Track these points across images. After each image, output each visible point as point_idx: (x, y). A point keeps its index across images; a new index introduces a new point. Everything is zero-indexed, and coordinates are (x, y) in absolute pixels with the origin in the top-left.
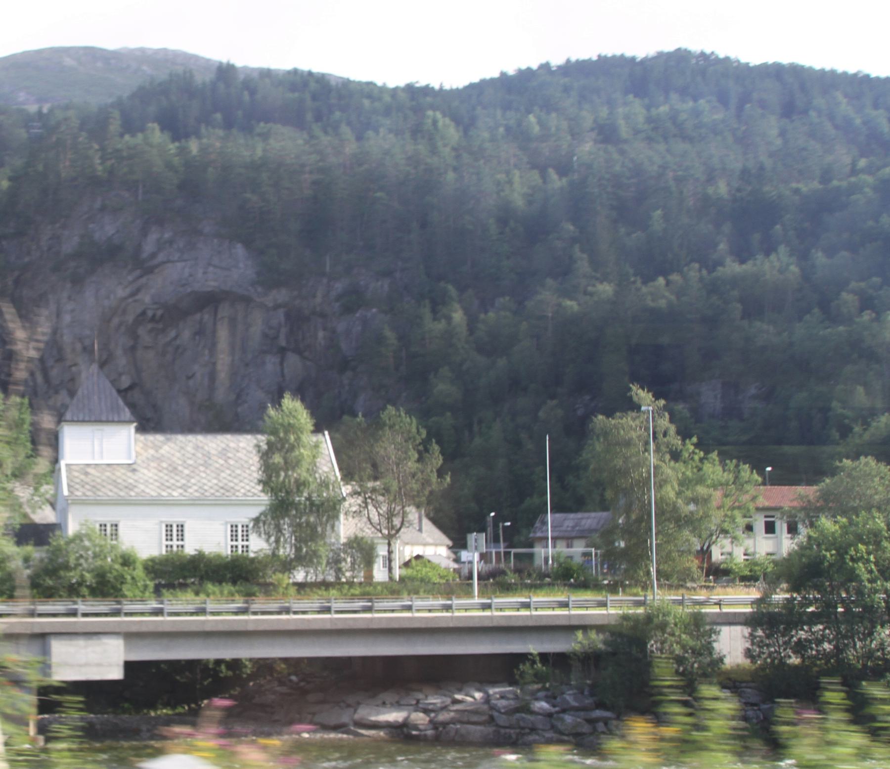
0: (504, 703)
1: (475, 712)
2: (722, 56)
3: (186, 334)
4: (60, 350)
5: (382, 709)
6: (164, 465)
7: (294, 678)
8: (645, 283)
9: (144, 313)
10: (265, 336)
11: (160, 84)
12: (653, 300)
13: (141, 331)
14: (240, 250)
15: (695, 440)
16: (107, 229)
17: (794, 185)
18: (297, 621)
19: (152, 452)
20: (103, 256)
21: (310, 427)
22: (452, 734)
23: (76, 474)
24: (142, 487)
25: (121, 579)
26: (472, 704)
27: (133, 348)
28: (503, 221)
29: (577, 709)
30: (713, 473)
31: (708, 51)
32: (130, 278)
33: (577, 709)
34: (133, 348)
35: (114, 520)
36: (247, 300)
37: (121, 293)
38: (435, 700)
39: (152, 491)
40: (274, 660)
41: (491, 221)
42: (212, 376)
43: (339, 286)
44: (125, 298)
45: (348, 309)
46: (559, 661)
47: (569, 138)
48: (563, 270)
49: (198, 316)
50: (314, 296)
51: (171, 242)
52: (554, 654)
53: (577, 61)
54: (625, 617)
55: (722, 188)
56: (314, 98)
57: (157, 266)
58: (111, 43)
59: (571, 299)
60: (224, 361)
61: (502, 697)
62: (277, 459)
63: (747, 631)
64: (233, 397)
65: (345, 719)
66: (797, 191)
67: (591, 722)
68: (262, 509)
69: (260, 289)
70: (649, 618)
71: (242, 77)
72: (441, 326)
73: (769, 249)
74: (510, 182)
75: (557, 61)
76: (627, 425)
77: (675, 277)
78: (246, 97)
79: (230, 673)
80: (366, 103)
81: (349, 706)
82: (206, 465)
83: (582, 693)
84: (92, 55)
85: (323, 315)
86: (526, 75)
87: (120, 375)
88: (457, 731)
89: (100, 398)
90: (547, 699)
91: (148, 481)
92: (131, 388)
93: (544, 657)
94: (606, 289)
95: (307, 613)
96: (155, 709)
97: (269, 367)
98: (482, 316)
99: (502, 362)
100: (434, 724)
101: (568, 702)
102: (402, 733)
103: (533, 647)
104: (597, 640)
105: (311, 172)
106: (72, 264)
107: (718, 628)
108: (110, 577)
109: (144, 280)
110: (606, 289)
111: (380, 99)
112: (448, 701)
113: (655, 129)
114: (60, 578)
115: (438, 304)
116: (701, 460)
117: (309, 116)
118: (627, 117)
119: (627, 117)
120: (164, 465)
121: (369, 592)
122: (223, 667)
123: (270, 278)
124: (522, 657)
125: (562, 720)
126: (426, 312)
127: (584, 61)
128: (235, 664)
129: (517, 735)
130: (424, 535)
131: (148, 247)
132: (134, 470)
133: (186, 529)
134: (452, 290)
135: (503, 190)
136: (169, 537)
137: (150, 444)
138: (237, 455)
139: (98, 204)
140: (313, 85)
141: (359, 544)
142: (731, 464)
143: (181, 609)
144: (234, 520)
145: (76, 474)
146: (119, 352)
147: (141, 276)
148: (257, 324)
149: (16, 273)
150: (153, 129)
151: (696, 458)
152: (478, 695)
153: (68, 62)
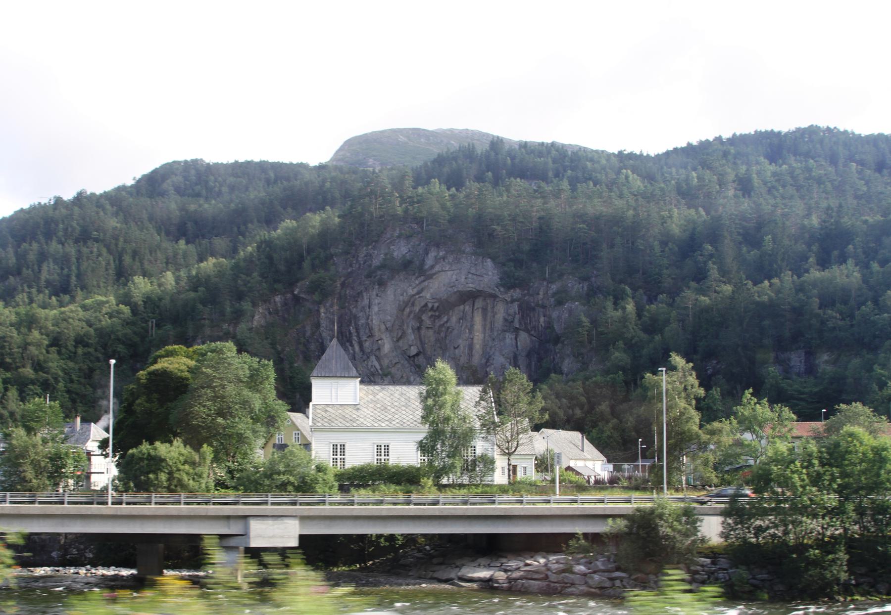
0: (556, 566)
1: (536, 572)
2: (842, 130)
3: (454, 319)
4: (371, 329)
5: (477, 569)
6: (379, 406)
7: (427, 547)
8: (755, 284)
9: (426, 305)
10: (506, 320)
11: (452, 153)
12: (759, 297)
13: (424, 317)
14: (489, 263)
15: (751, 390)
16: (401, 250)
17: (864, 218)
18: (440, 510)
19: (371, 397)
20: (409, 267)
21: (454, 380)
22: (519, 586)
23: (319, 411)
24: (362, 420)
25: (315, 481)
26: (537, 566)
27: (419, 329)
28: (664, 244)
29: (604, 571)
30: (763, 413)
31: (832, 127)
32: (417, 282)
33: (604, 571)
34: (419, 329)
35: (342, 442)
36: (494, 297)
37: (411, 292)
38: (513, 564)
39: (368, 423)
40: (59, 534)
41: (656, 243)
42: (471, 347)
43: (554, 287)
44: (414, 295)
45: (560, 303)
46: (594, 538)
47: (718, 187)
48: (700, 276)
49: (462, 307)
50: (538, 294)
51: (444, 258)
52: (592, 534)
53: (741, 135)
54: (638, 510)
55: (815, 221)
56: (554, 162)
57: (434, 274)
58: (431, 126)
59: (704, 295)
60: (478, 337)
61: (557, 562)
62: (430, 402)
63: (720, 519)
64: (484, 361)
65: (453, 575)
66: (866, 222)
67: (612, 579)
68: (424, 435)
69: (502, 289)
70: (652, 511)
71: (507, 147)
72: (619, 313)
73: (843, 260)
74: (671, 217)
75: (726, 135)
76: (664, 380)
77: (775, 281)
78: (509, 161)
79: (387, 544)
80: (589, 164)
81: (457, 567)
82: (406, 406)
83: (609, 560)
84: (417, 133)
85: (544, 307)
86: (705, 145)
87: (410, 346)
88: (523, 584)
89: (336, 362)
90: (585, 564)
91: (366, 416)
92: (417, 355)
93: (586, 535)
94: (728, 289)
95: (448, 504)
96: (338, 567)
97: (508, 341)
98: (647, 307)
99: (658, 338)
100: (509, 580)
101: (598, 566)
102: (488, 586)
103: (579, 528)
104: (622, 524)
105: (538, 211)
106: (379, 273)
107: (701, 517)
108: (308, 479)
109: (426, 283)
110: (728, 289)
111: (598, 162)
112: (521, 564)
113: (778, 181)
114: (273, 479)
115: (618, 299)
116: (755, 404)
117: (550, 174)
118: (759, 173)
119: (759, 173)
120: (379, 406)
121: (489, 492)
122: (382, 540)
123: (508, 282)
124: (572, 536)
125: (592, 578)
126: (609, 304)
127: (745, 135)
128: (391, 538)
129: (553, 589)
130: (585, 454)
131: (429, 262)
132: (358, 409)
133: (346, 447)
134: (629, 290)
135: (665, 222)
136: (379, 453)
137: (370, 392)
138: (404, 401)
139: (396, 233)
140: (554, 152)
141: (483, 459)
142: (777, 407)
143: (365, 502)
144: (335, 442)
145: (319, 411)
146: (410, 331)
147: (424, 281)
148: (501, 311)
149: (343, 279)
150: (435, 183)
151: (752, 402)
152: (542, 561)
153: (402, 138)
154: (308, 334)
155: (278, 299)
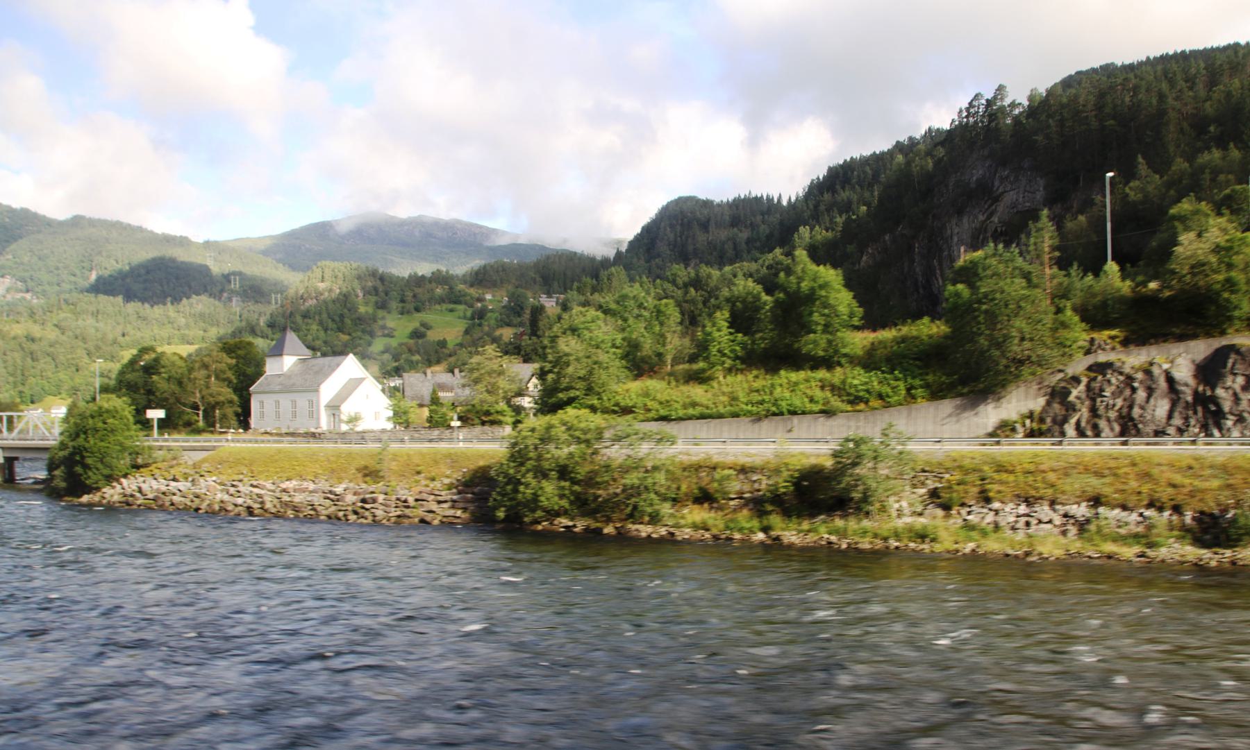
9: (996, 230)
37: (981, 218)
51: (1007, 177)
131: (997, 183)
154: (906, 269)
155: (887, 238)
